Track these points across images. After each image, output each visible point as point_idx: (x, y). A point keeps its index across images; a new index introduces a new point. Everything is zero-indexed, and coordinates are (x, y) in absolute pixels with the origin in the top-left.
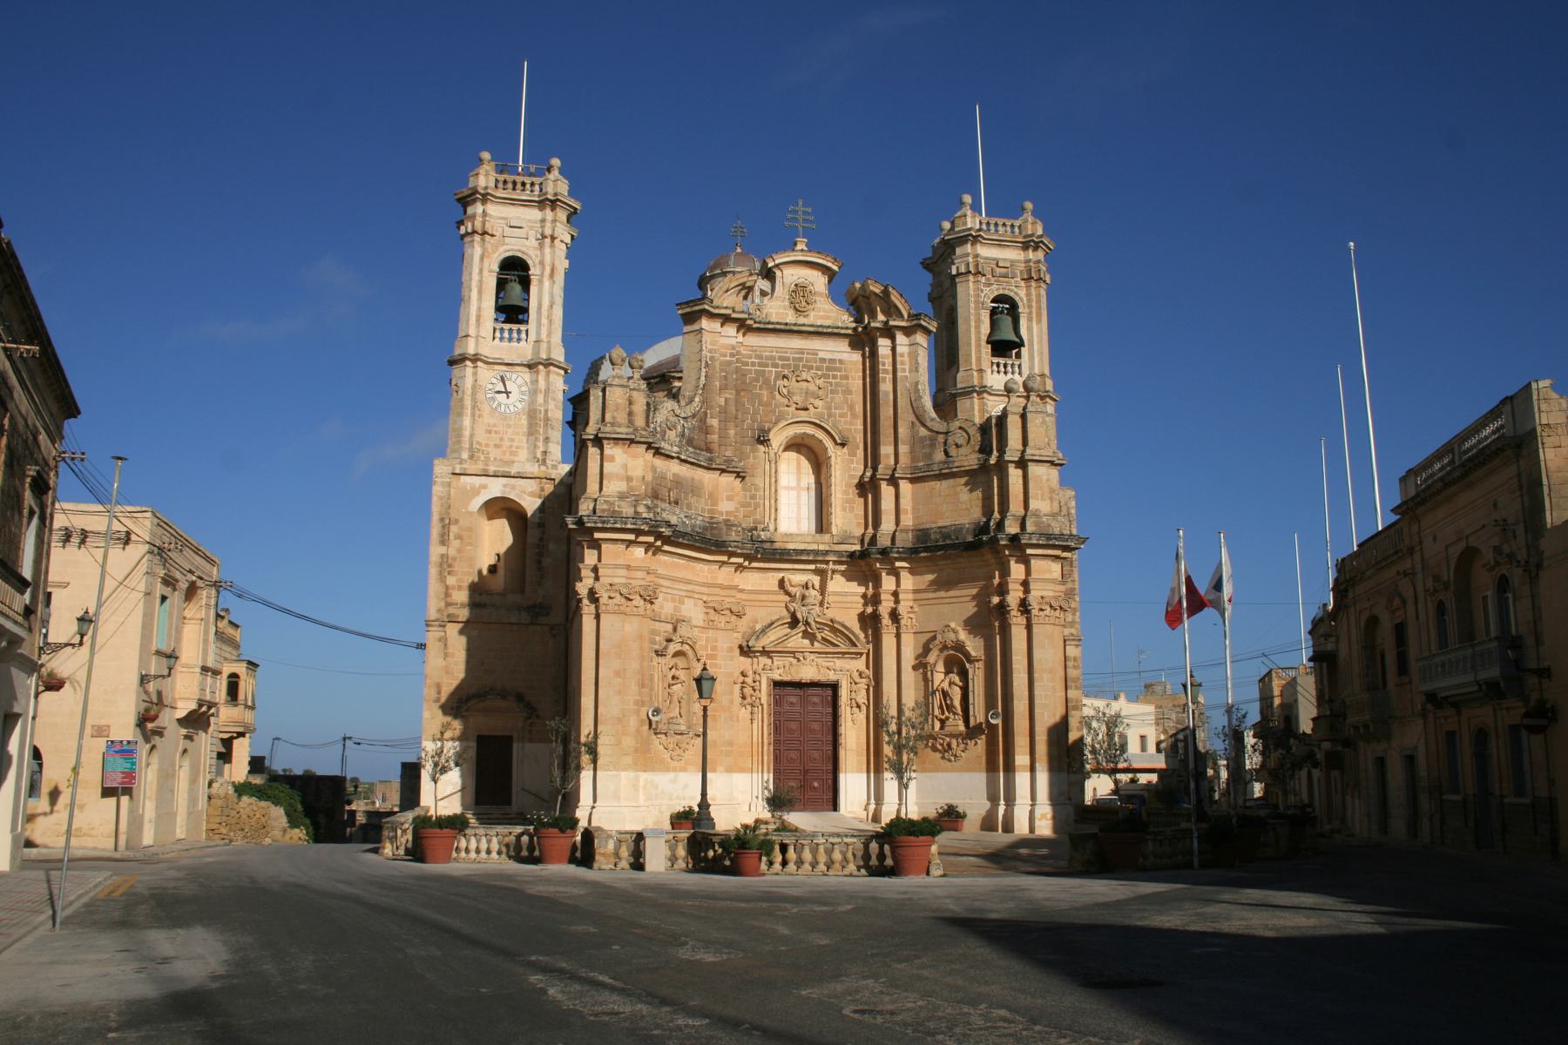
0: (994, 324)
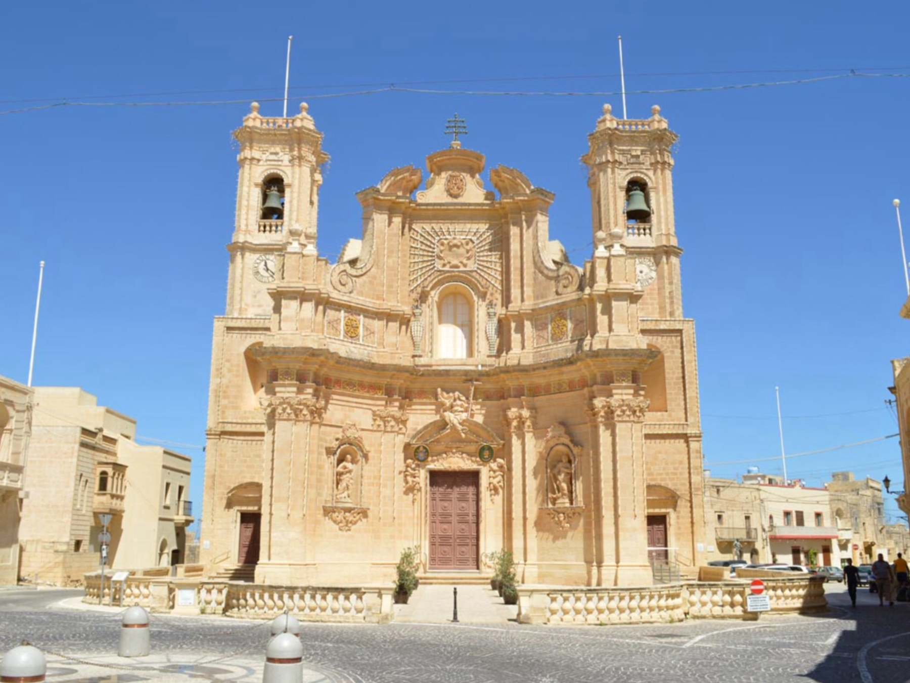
0: (265, 197)
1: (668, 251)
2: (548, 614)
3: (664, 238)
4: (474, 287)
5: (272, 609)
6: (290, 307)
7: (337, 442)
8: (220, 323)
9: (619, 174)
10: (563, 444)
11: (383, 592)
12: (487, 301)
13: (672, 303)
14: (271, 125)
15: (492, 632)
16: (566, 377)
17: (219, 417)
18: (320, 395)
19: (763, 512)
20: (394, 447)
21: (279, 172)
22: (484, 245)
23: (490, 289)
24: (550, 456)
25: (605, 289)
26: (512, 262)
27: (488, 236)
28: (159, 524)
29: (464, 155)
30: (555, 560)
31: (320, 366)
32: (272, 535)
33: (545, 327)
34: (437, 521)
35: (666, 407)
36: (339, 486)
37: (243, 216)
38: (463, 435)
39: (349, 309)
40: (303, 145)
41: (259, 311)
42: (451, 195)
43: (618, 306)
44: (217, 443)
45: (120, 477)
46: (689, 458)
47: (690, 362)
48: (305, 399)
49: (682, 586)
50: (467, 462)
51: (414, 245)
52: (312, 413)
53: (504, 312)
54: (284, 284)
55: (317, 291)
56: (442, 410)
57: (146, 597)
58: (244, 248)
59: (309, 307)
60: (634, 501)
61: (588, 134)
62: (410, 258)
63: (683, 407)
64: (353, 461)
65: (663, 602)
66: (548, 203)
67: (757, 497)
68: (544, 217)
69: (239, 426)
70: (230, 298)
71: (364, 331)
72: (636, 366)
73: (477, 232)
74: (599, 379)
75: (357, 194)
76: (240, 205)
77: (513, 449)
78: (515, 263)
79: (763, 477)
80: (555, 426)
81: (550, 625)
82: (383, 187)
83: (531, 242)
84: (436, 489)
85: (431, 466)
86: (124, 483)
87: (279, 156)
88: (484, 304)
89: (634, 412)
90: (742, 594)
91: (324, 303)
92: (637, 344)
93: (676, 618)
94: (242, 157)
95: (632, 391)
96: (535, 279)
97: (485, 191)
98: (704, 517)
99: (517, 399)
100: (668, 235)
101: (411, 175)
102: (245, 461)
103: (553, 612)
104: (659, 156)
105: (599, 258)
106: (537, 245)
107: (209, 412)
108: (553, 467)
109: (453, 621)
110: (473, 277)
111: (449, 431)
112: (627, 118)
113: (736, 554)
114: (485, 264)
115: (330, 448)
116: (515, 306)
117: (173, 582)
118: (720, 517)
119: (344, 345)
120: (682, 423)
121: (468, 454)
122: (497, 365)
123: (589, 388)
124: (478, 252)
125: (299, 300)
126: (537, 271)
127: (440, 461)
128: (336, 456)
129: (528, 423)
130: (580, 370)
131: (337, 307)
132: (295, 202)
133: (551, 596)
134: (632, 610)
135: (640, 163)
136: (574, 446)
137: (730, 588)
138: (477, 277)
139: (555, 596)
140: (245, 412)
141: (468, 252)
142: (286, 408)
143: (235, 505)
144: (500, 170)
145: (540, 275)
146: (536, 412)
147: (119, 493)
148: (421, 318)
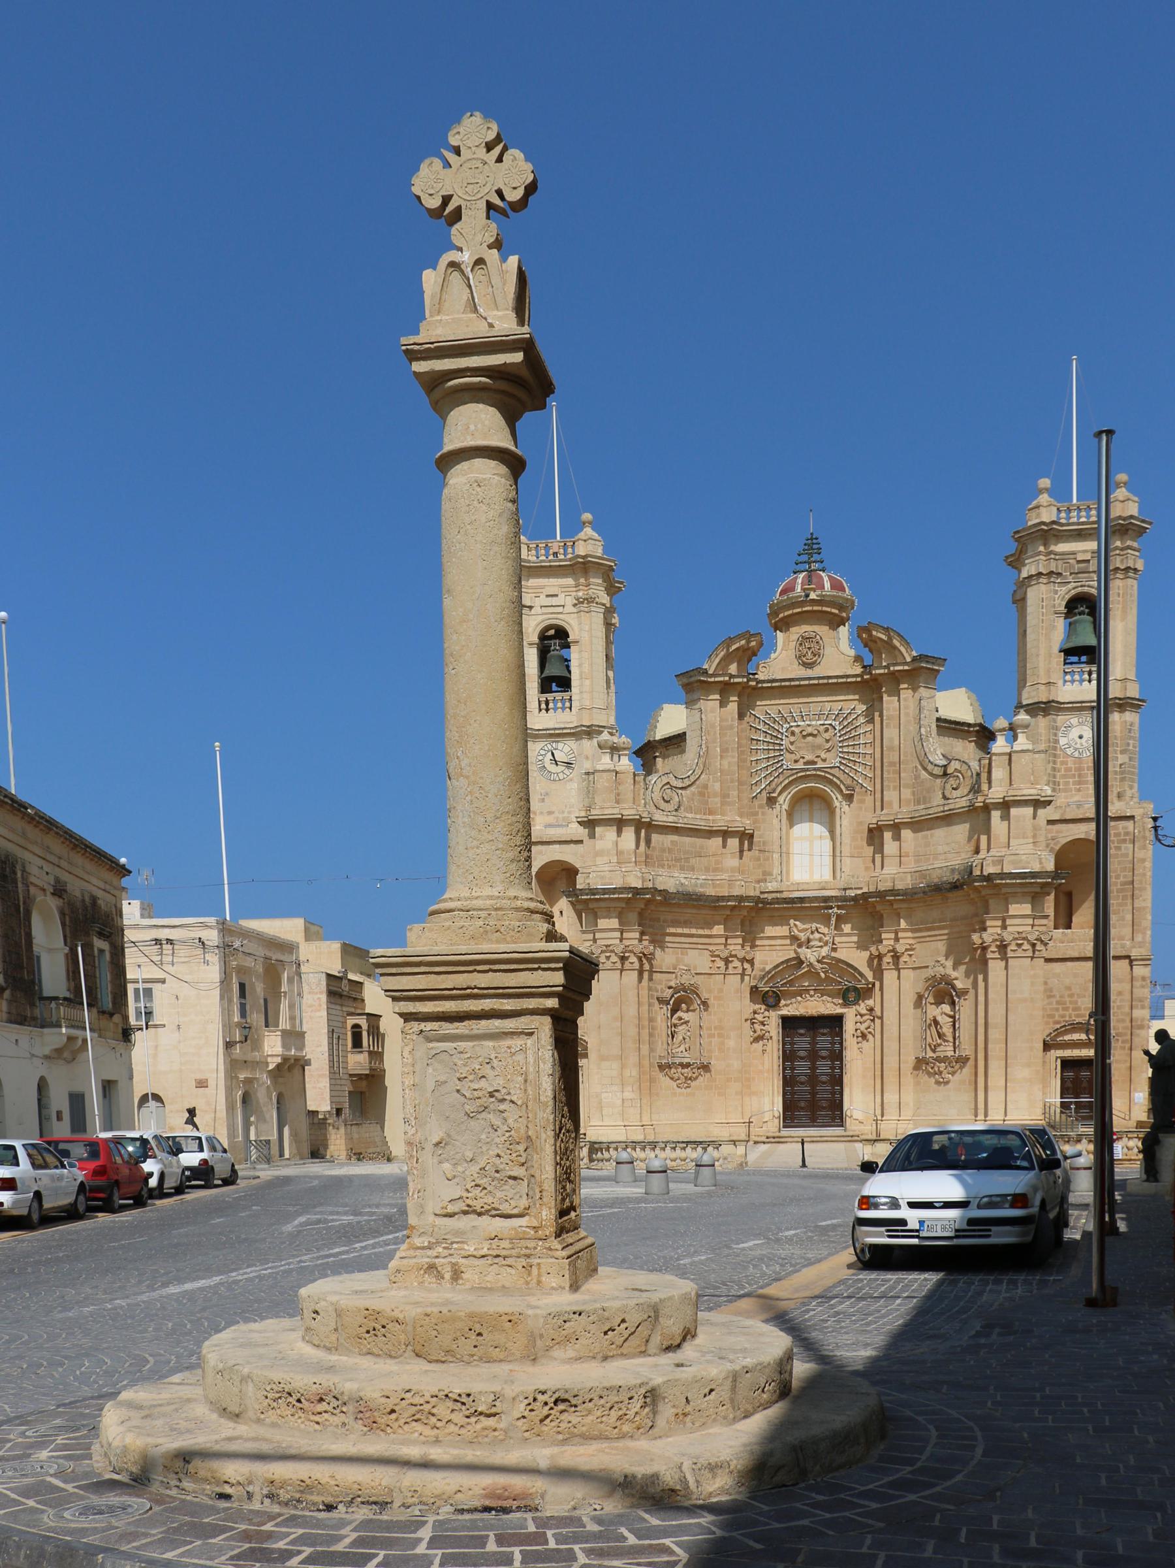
66: (938, 671)
85: (785, 1012)
92: (1041, 863)
112: (1078, 500)
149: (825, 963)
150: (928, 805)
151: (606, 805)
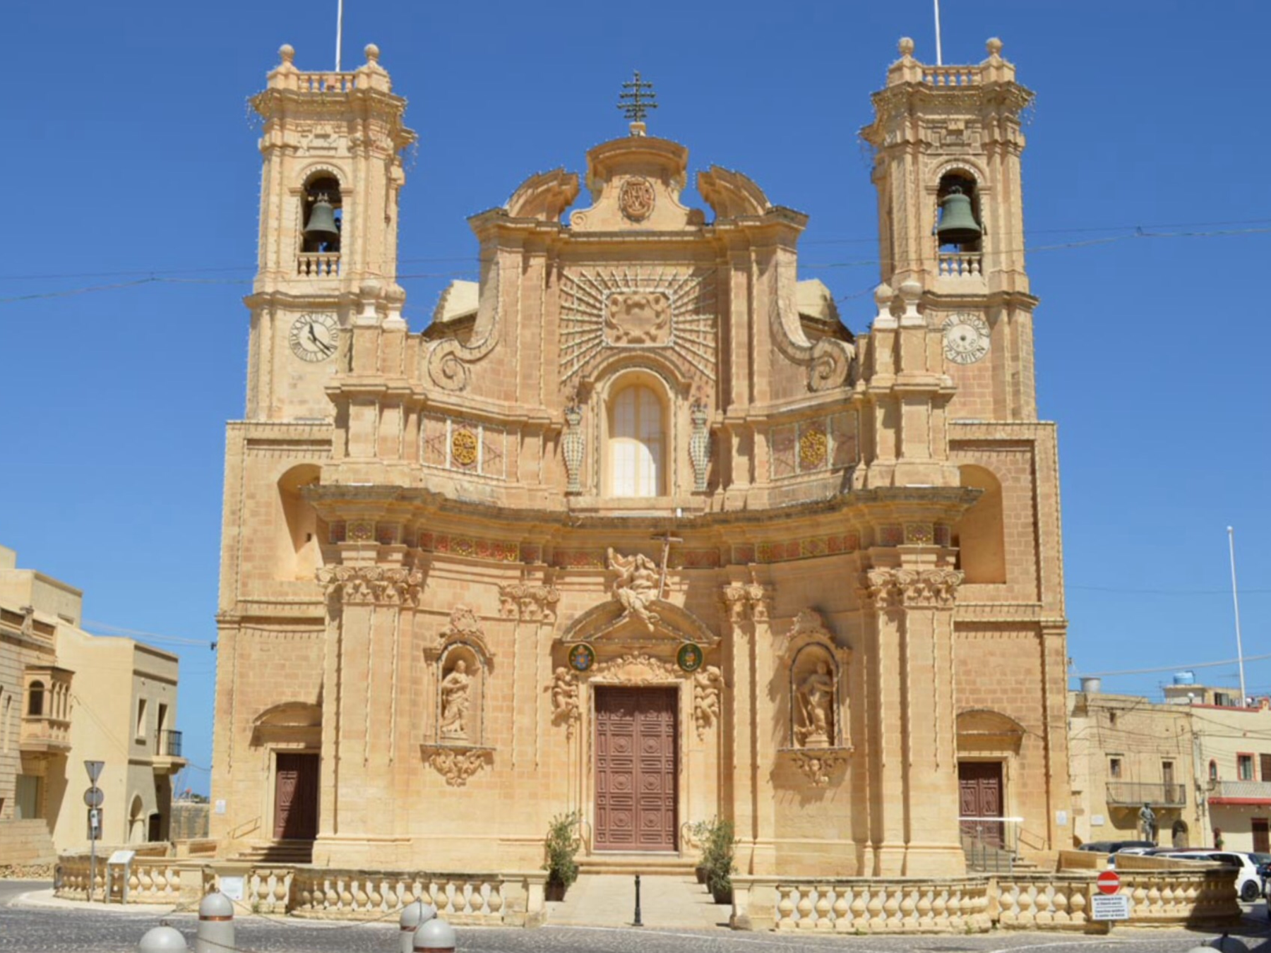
0: (308, 211)
1: (1011, 301)
2: (777, 917)
3: (1004, 277)
4: (669, 375)
5: (364, 905)
6: (363, 417)
7: (443, 640)
8: (236, 432)
9: (926, 165)
10: (819, 644)
11: (529, 880)
12: (692, 399)
13: (1017, 393)
14: (316, 85)
15: (691, 939)
16: (823, 532)
17: (239, 592)
18: (414, 563)
19: (1196, 753)
20: (536, 648)
21: (330, 168)
22: (686, 304)
23: (697, 378)
24: (797, 662)
25: (889, 384)
26: (734, 332)
27: (694, 287)
28: (129, 771)
29: (653, 148)
30: (805, 837)
31: (414, 515)
32: (340, 791)
33: (789, 445)
34: (608, 770)
35: (1004, 575)
36: (446, 712)
37: (272, 247)
38: (651, 627)
39: (462, 418)
40: (371, 121)
41: (302, 411)
42: (630, 217)
43: (911, 413)
44: (235, 636)
45: (63, 690)
46: (1043, 664)
47: (1047, 496)
48: (389, 570)
49: (987, 879)
50: (658, 672)
51: (566, 305)
52: (401, 592)
53: (720, 418)
54: (353, 381)
55: (408, 391)
56: (615, 585)
57: (147, 888)
58: (275, 303)
59: (394, 416)
60: (935, 741)
61: (871, 92)
62: (559, 326)
63: (1034, 575)
64: (469, 671)
65: (955, 902)
66: (797, 230)
67: (1187, 728)
68: (788, 255)
69: (271, 607)
70: (252, 390)
71: (484, 453)
72: (943, 515)
73: (674, 280)
74: (878, 537)
75: (469, 218)
76: (266, 228)
77: (735, 651)
78: (738, 336)
79: (1201, 692)
80: (804, 613)
81: (779, 932)
82: (513, 208)
83: (766, 300)
84: (604, 716)
85: (598, 679)
86: (69, 699)
87: (330, 140)
88: (686, 404)
89: (938, 592)
90: (1085, 893)
91: (418, 408)
92: (944, 477)
93: (975, 926)
94: (267, 144)
95: (933, 558)
96: (773, 363)
97: (688, 209)
98: (1068, 765)
99: (741, 568)
100: (1011, 273)
101: (561, 185)
102: (283, 666)
103: (785, 914)
104: (997, 131)
105: (880, 330)
106: (777, 303)
107: (220, 585)
108: (802, 681)
109: (633, 925)
110: (666, 358)
111: (627, 619)
112: (943, 62)
113: (1144, 830)
114: (687, 336)
115: (431, 649)
116: (739, 408)
117: (212, 865)
118: (1115, 763)
119: (452, 479)
120: (1031, 603)
121: (659, 658)
122: (707, 510)
123: (863, 552)
124: (676, 316)
125: (377, 407)
126: (776, 349)
127: (612, 669)
128: (441, 664)
129: (760, 608)
130: (848, 520)
131: (439, 415)
132: (360, 221)
133: (781, 889)
134: (906, 913)
135: (963, 145)
136: (837, 647)
137: (1065, 884)
138: (675, 358)
139: (787, 889)
140: (281, 584)
141: (658, 314)
142: (360, 585)
143: (267, 742)
144: (714, 175)
145: (782, 356)
146: (774, 590)
147: (61, 718)
148: (579, 429)
149: (654, 611)
150: (790, 399)
151: (366, 373)
